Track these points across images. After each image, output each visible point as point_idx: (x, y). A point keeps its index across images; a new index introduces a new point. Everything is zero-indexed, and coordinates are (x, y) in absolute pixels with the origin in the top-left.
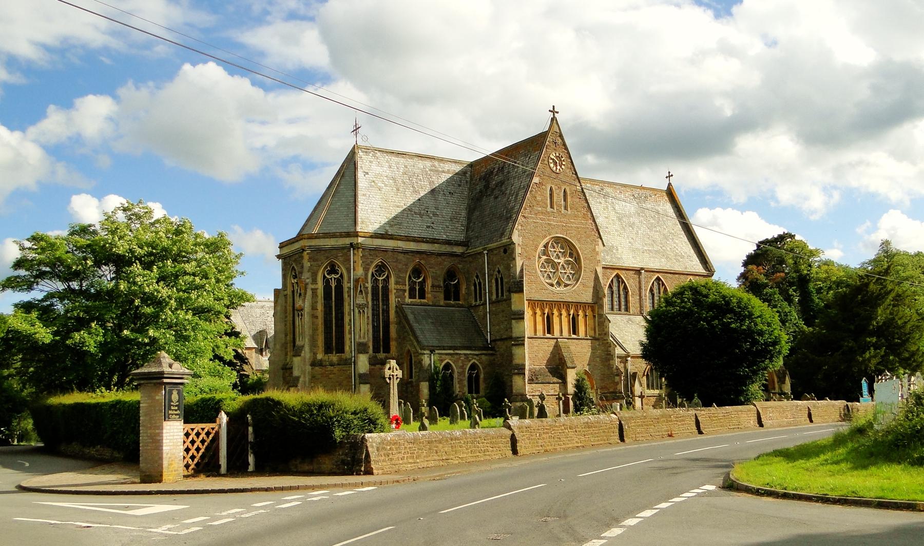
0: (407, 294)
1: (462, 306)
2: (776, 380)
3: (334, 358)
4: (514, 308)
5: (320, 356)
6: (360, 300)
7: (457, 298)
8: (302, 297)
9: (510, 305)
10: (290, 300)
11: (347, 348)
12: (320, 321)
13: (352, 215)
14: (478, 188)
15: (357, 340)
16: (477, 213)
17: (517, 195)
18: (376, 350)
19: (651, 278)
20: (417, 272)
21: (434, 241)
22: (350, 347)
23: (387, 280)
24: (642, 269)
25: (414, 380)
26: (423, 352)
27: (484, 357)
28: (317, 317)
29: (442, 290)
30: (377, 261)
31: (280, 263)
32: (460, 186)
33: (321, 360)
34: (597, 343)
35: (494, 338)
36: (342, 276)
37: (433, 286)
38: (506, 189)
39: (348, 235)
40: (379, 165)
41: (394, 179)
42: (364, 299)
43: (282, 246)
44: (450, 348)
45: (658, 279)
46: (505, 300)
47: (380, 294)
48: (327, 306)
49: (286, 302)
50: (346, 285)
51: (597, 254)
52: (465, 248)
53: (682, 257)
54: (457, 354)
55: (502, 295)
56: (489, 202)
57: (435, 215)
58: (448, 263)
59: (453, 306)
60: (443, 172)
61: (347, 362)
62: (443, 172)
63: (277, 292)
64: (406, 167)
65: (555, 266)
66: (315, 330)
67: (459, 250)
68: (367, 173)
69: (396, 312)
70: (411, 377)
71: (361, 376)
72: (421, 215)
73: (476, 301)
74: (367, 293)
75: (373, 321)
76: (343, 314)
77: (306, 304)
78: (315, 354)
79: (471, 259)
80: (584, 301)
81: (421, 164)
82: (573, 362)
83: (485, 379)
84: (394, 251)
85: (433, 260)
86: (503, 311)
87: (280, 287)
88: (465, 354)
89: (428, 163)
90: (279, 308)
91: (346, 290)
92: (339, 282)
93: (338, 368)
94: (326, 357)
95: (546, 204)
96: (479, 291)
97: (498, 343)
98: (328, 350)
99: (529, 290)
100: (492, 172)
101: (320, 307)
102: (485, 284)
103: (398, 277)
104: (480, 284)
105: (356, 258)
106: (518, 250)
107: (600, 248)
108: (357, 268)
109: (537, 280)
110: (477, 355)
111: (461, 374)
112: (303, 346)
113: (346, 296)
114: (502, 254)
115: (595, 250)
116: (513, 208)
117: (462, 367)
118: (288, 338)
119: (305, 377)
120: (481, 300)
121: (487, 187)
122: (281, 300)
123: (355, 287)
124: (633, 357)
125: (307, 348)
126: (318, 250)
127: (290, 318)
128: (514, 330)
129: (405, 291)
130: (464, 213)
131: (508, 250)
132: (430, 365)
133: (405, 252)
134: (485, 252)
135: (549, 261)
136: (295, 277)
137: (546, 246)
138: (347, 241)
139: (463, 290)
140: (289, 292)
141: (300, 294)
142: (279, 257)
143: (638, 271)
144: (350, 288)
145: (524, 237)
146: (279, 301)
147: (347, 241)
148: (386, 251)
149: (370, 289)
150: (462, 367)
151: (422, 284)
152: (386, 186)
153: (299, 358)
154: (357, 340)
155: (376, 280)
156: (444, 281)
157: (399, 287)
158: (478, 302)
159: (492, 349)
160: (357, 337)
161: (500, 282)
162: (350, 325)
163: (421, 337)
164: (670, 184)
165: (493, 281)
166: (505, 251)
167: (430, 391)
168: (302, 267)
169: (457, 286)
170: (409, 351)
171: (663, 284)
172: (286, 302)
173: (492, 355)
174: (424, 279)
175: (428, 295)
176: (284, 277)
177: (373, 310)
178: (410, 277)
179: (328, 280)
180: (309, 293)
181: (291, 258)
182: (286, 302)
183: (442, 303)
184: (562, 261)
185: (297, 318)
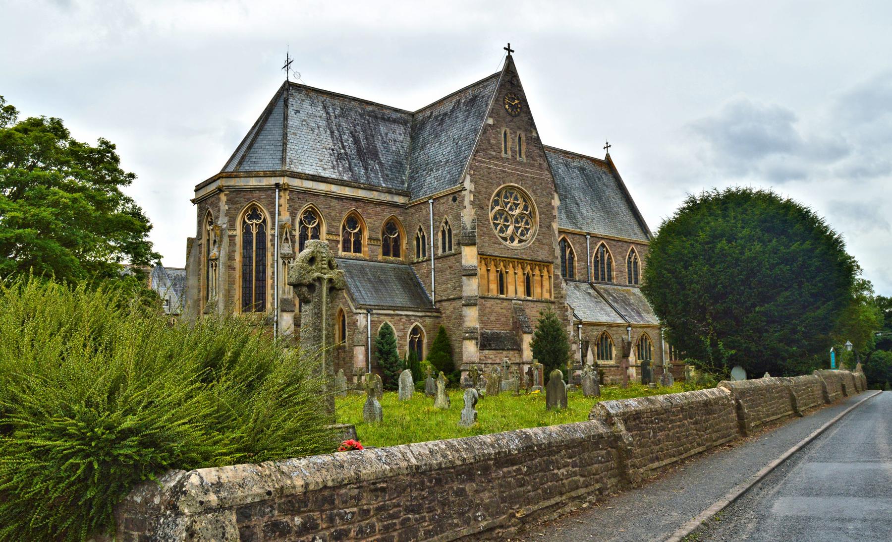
0: (340, 246)
3: (254, 316)
7: (397, 255)
8: (217, 245)
9: (459, 261)
10: (204, 250)
11: (269, 306)
12: (238, 274)
19: (596, 244)
20: (352, 221)
24: (588, 234)
25: (346, 344)
26: (359, 311)
27: (428, 320)
28: (234, 269)
29: (381, 243)
31: (195, 208)
35: (439, 298)
36: (264, 221)
37: (370, 239)
39: (274, 174)
43: (198, 188)
45: (603, 245)
46: (454, 255)
50: (269, 232)
54: (398, 315)
55: (450, 249)
58: (387, 214)
59: (392, 263)
61: (269, 323)
63: (190, 241)
66: (231, 282)
68: (298, 112)
73: (418, 257)
74: (293, 242)
76: (264, 266)
79: (413, 210)
83: (429, 344)
84: (327, 195)
85: (370, 209)
86: (451, 267)
87: (194, 235)
88: (407, 316)
90: (192, 260)
91: (269, 238)
92: (262, 227)
94: (244, 315)
96: (421, 244)
97: (444, 303)
98: (246, 305)
101: (238, 257)
102: (429, 238)
103: (330, 226)
104: (423, 237)
105: (282, 200)
110: (420, 317)
113: (269, 244)
114: (451, 202)
115: (550, 204)
120: (424, 255)
123: (281, 235)
125: (221, 305)
126: (239, 191)
127: (203, 272)
128: (464, 288)
129: (338, 242)
132: (366, 327)
133: (340, 198)
134: (431, 201)
136: (211, 223)
140: (204, 241)
142: (193, 201)
144: (273, 235)
146: (193, 251)
147: (273, 181)
148: (316, 195)
149: (297, 238)
150: (404, 330)
155: (306, 228)
156: (383, 234)
158: (421, 259)
160: (280, 292)
161: (447, 234)
162: (273, 278)
163: (357, 295)
164: (608, 156)
165: (440, 234)
166: (454, 200)
168: (219, 210)
169: (397, 241)
170: (341, 310)
171: (607, 251)
172: (200, 253)
173: (437, 317)
175: (365, 249)
176: (200, 223)
178: (344, 228)
179: (248, 225)
180: (226, 240)
181: (206, 199)
183: (380, 257)
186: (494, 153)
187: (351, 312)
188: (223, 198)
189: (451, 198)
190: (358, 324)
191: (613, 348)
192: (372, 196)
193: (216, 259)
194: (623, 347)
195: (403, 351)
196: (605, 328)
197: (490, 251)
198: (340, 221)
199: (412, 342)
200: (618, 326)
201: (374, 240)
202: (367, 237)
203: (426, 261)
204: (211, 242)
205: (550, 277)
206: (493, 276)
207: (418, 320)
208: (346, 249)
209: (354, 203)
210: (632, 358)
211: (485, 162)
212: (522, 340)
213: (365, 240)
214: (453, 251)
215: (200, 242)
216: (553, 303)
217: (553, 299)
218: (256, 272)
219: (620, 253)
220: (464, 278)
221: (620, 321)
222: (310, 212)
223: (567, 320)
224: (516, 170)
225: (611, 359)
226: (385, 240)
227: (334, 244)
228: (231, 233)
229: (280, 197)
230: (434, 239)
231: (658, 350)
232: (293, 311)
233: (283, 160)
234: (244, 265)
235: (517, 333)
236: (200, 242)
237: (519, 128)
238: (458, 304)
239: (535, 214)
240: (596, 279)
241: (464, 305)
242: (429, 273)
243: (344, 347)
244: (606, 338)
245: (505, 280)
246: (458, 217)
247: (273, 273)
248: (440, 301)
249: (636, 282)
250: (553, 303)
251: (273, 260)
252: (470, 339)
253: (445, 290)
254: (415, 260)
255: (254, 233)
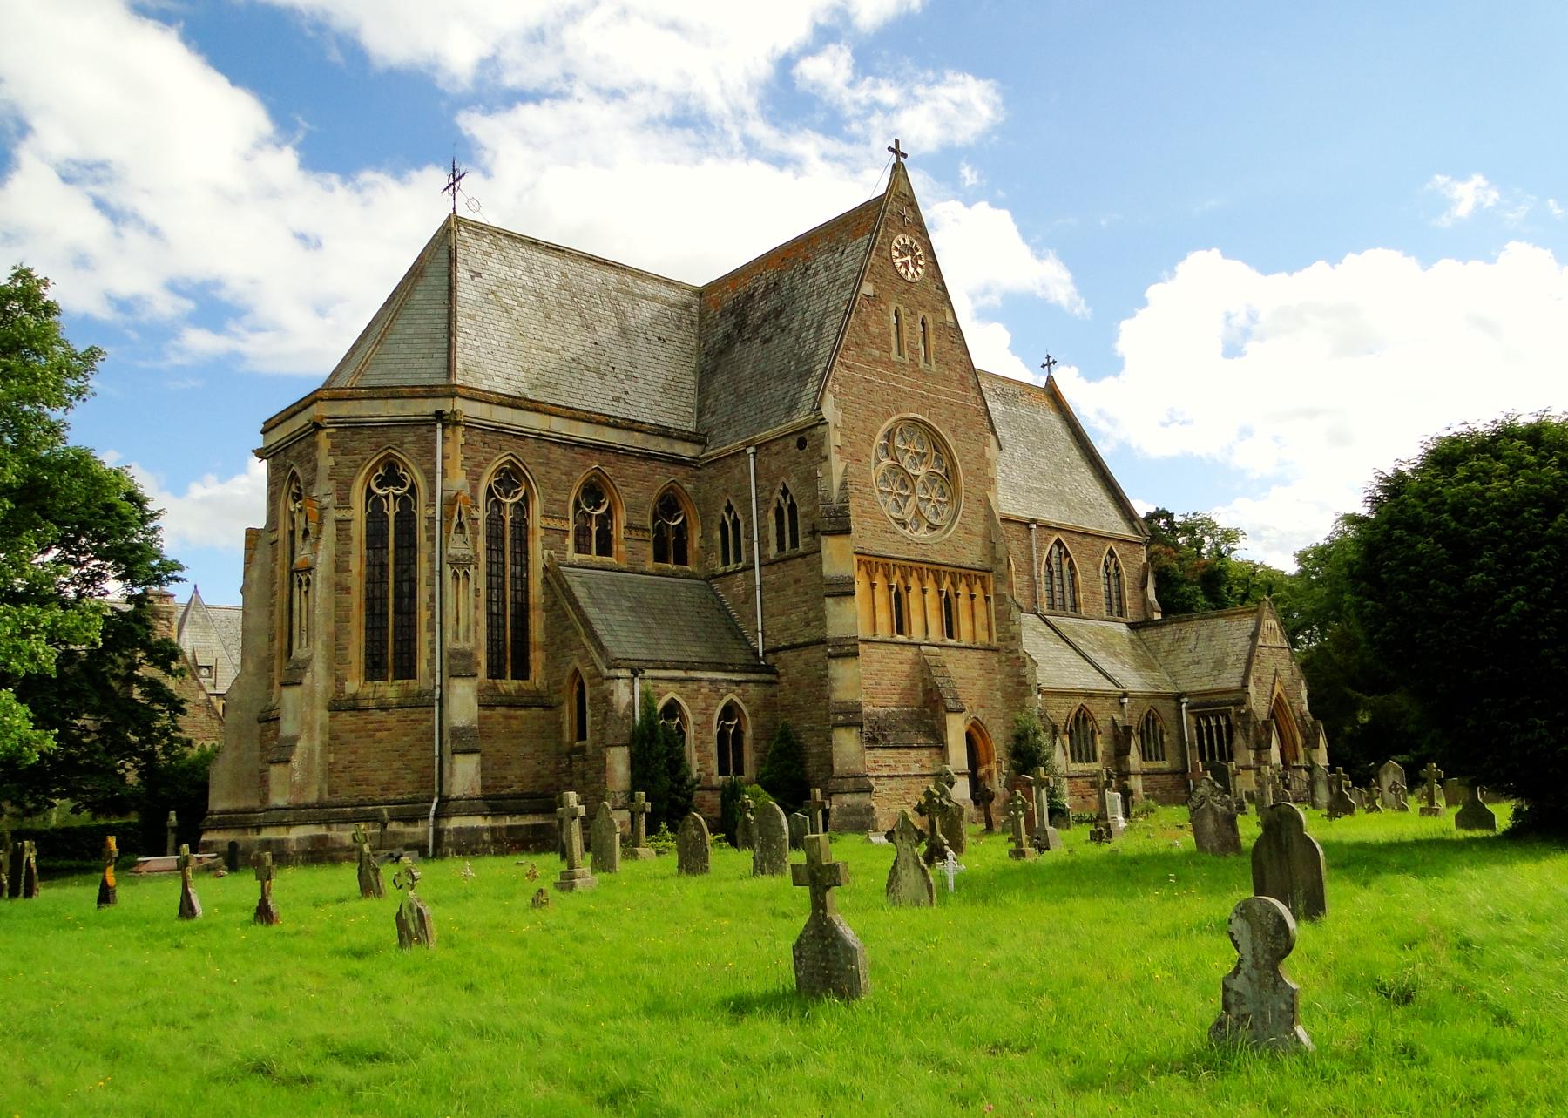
0: (570, 541)
1: (691, 576)
2: (1299, 740)
3: (390, 689)
4: (829, 570)
5: (353, 686)
6: (458, 547)
7: (681, 559)
8: (311, 538)
10: (283, 553)
11: (422, 666)
12: (356, 600)
13: (441, 357)
14: (720, 332)
15: (450, 643)
16: (721, 378)
17: (820, 327)
18: (496, 671)
20: (593, 492)
21: (631, 426)
22: (431, 662)
23: (522, 507)
24: (1034, 521)
25: (588, 742)
26: (613, 673)
27: (751, 688)
28: (347, 590)
29: (651, 536)
30: (499, 460)
32: (679, 328)
33: (355, 697)
34: (995, 658)
35: (772, 644)
36: (413, 490)
37: (629, 527)
38: (791, 321)
39: (430, 392)
40: (504, 260)
41: (540, 297)
42: (471, 546)
44: (678, 665)
45: (1059, 543)
46: (803, 556)
47: (507, 539)
48: (375, 570)
49: (273, 558)
50: (422, 512)
51: (988, 464)
52: (699, 448)
53: (1092, 506)
54: (693, 680)
55: (794, 543)
56: (750, 355)
57: (630, 377)
58: (662, 478)
59: (674, 575)
60: (644, 297)
62: (644, 297)
63: (252, 535)
64: (564, 275)
65: (907, 481)
66: (341, 620)
67: (686, 450)
68: (479, 275)
69: (546, 582)
70: (582, 735)
71: (457, 733)
72: (601, 375)
73: (726, 562)
74: (475, 533)
75: (489, 601)
76: (413, 582)
77: (322, 558)
78: (340, 681)
79: (712, 471)
80: (968, 563)
81: (597, 275)
82: (956, 699)
83: (756, 740)
84: (541, 438)
85: (629, 468)
86: (797, 581)
87: (260, 523)
88: (712, 681)
89: (613, 277)
90: (255, 574)
91: (422, 524)
92: (406, 505)
93: (399, 713)
94: (369, 688)
95: (888, 343)
96: (732, 539)
97: (782, 655)
98: (374, 669)
99: (866, 533)
100: (751, 296)
101: (357, 564)
104: (736, 523)
105: (450, 448)
106: (835, 439)
107: (992, 451)
108: (453, 474)
109: (884, 513)
110: (738, 683)
111: (703, 727)
112: (309, 660)
113: (422, 537)
115: (983, 455)
116: (812, 354)
117: (705, 711)
118: (277, 644)
119: (311, 738)
120: (738, 559)
121: (740, 326)
122: (262, 554)
123: (447, 517)
124: (1044, 694)
126: (355, 426)
128: (830, 622)
129: (566, 532)
130: (690, 381)
131: (807, 440)
132: (631, 705)
133: (568, 444)
134: (751, 450)
135: (896, 468)
136: (298, 497)
137: (889, 435)
138: (428, 407)
139: (695, 540)
140: (282, 534)
141: (306, 532)
143: (1026, 524)
144: (431, 519)
145: (845, 410)
146: (257, 556)
147: (428, 407)
148: (522, 437)
150: (705, 711)
151: (605, 521)
152: (521, 305)
153: (296, 690)
154: (450, 643)
157: (552, 524)
158: (731, 567)
159: (770, 669)
160: (449, 636)
161: (787, 517)
162: (431, 608)
163: (607, 640)
164: (1050, 379)
165: (771, 515)
166: (802, 444)
167: (632, 768)
168: (315, 469)
169: (681, 531)
170: (577, 671)
171: (1067, 555)
172: (274, 559)
174: (609, 510)
175: (619, 547)
176: (273, 499)
177: (489, 574)
178: (577, 505)
179: (378, 498)
180: (330, 529)
182: (274, 559)
183: (650, 565)
184: (921, 471)
185: (296, 590)
186: (877, 353)
187: (599, 674)
188: (323, 441)
189: (793, 442)
190: (614, 699)
191: (1098, 739)
192: (631, 442)
193: (309, 569)
194: (1116, 737)
195: (700, 759)
196: (1081, 701)
197: (876, 547)
198: (568, 490)
199: (722, 736)
200: (1105, 695)
201: (636, 529)
202: (623, 524)
203: (744, 569)
204: (299, 534)
205: (987, 599)
206: (881, 598)
207: (741, 692)
208: (581, 547)
209: (597, 455)
210: (1134, 759)
211: (861, 369)
212: (944, 726)
213: (619, 530)
214: (801, 548)
215: (273, 537)
216: (996, 650)
217: (995, 643)
218: (396, 596)
219: (1090, 557)
220: (829, 601)
221: (1107, 686)
222: (507, 472)
223: (1024, 683)
224: (919, 387)
225: (1095, 760)
226: (659, 531)
227: (557, 537)
228: (340, 515)
229: (445, 438)
230: (759, 527)
231: (1175, 740)
232: (474, 676)
233: (450, 368)
234: (370, 581)
235: (935, 711)
236: (273, 537)
237: (922, 305)
238: (816, 654)
239: (956, 475)
240: (1052, 606)
241: (831, 656)
242: (750, 595)
243: (583, 749)
244: (1085, 720)
245: (904, 603)
246: (810, 479)
247: (432, 597)
248: (775, 651)
249: (1121, 613)
250: (996, 650)
251: (433, 570)
252: (847, 725)
253: (785, 628)
254: (721, 569)
255: (391, 515)
